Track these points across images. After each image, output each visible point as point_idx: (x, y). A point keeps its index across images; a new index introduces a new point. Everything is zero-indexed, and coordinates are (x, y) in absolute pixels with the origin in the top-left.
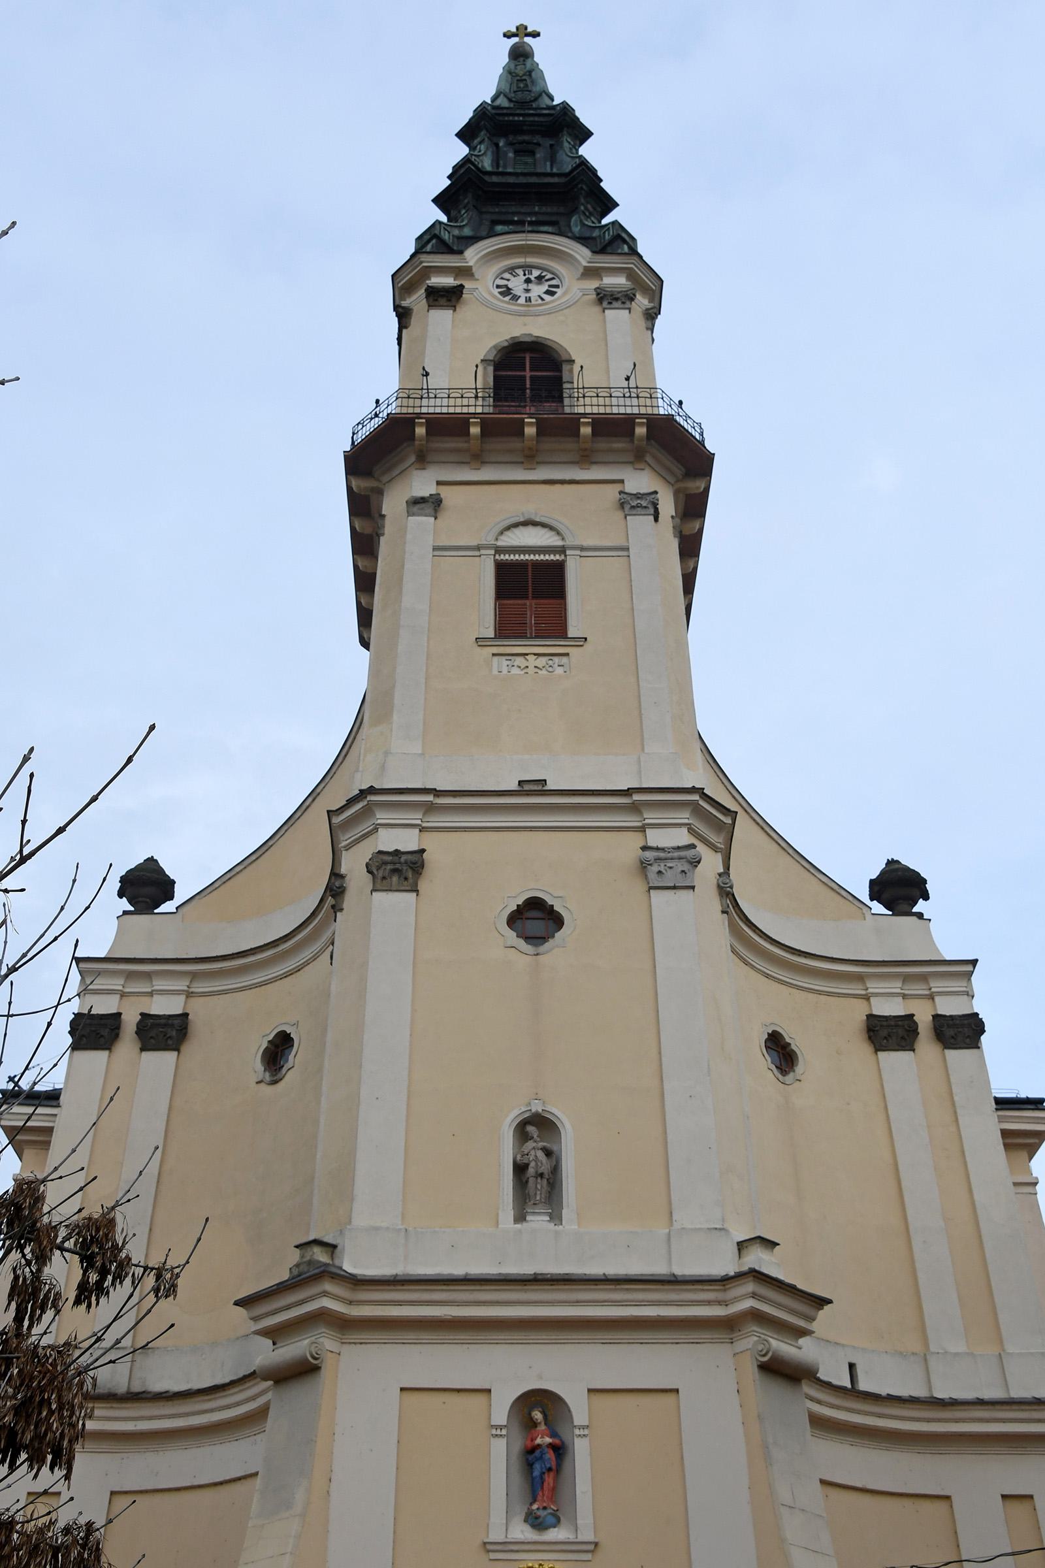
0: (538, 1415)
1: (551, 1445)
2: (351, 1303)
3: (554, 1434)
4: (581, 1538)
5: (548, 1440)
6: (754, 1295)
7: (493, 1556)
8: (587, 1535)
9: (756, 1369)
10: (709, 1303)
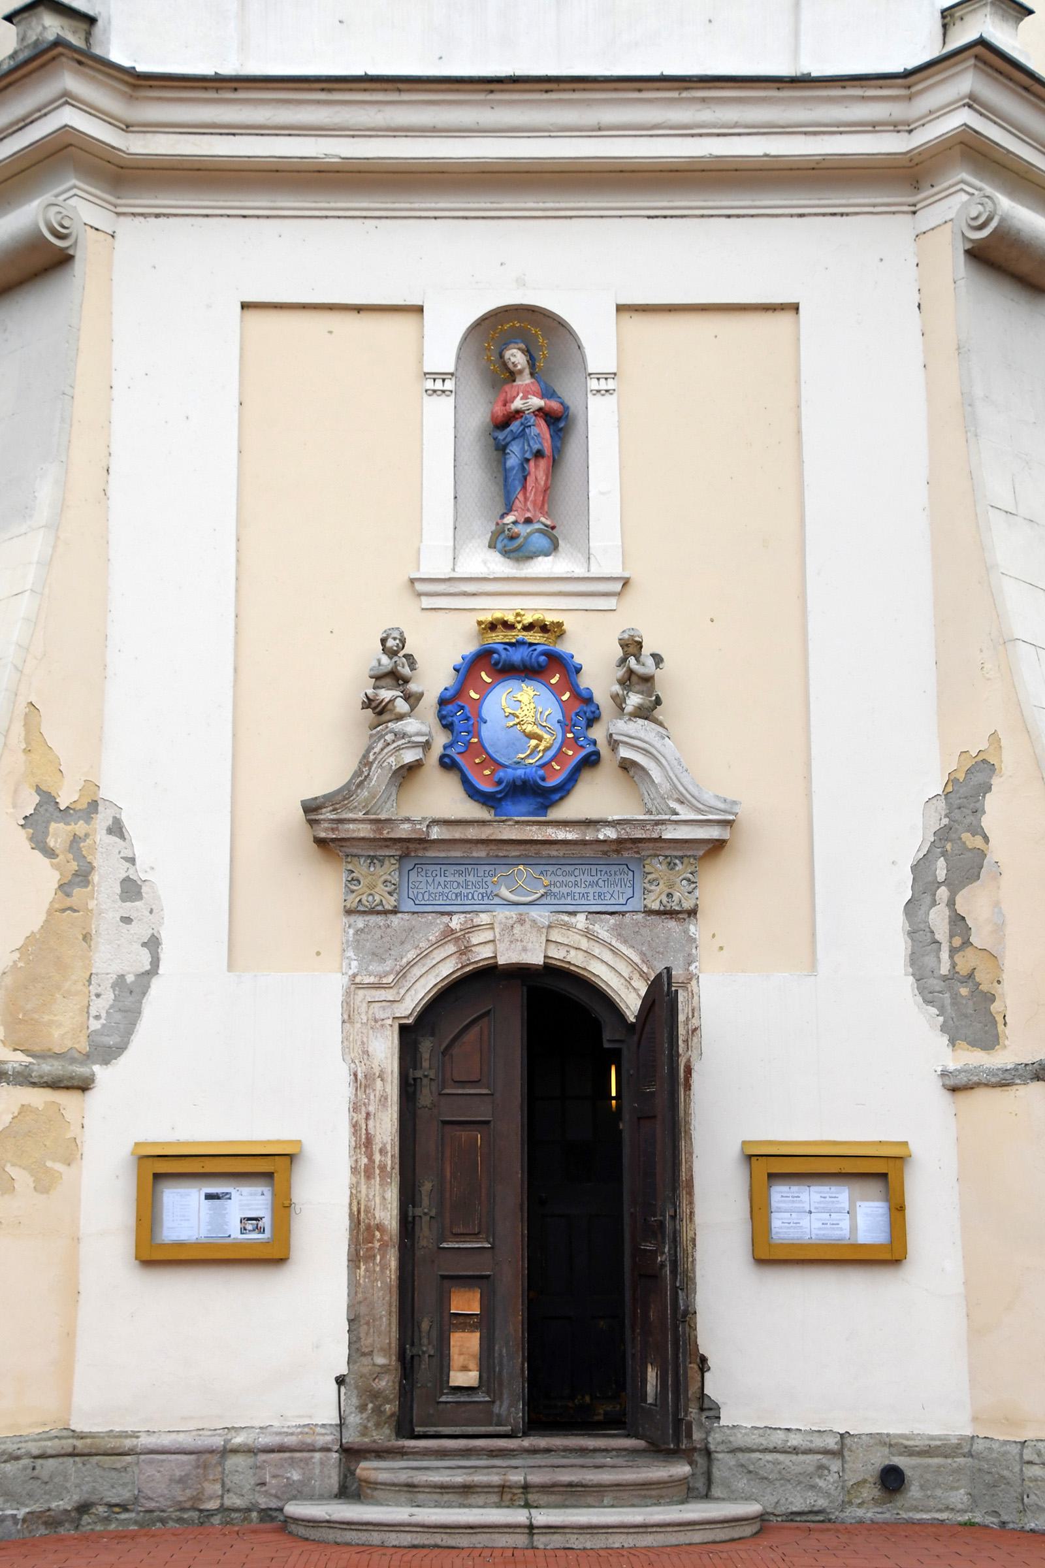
0: (516, 357)
1: (541, 412)
2: (127, 127)
3: (547, 393)
4: (595, 571)
5: (536, 402)
6: (972, 102)
7: (427, 602)
8: (607, 564)
9: (961, 257)
10: (873, 127)
